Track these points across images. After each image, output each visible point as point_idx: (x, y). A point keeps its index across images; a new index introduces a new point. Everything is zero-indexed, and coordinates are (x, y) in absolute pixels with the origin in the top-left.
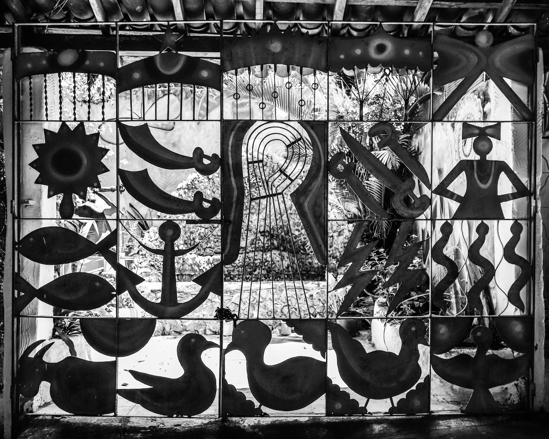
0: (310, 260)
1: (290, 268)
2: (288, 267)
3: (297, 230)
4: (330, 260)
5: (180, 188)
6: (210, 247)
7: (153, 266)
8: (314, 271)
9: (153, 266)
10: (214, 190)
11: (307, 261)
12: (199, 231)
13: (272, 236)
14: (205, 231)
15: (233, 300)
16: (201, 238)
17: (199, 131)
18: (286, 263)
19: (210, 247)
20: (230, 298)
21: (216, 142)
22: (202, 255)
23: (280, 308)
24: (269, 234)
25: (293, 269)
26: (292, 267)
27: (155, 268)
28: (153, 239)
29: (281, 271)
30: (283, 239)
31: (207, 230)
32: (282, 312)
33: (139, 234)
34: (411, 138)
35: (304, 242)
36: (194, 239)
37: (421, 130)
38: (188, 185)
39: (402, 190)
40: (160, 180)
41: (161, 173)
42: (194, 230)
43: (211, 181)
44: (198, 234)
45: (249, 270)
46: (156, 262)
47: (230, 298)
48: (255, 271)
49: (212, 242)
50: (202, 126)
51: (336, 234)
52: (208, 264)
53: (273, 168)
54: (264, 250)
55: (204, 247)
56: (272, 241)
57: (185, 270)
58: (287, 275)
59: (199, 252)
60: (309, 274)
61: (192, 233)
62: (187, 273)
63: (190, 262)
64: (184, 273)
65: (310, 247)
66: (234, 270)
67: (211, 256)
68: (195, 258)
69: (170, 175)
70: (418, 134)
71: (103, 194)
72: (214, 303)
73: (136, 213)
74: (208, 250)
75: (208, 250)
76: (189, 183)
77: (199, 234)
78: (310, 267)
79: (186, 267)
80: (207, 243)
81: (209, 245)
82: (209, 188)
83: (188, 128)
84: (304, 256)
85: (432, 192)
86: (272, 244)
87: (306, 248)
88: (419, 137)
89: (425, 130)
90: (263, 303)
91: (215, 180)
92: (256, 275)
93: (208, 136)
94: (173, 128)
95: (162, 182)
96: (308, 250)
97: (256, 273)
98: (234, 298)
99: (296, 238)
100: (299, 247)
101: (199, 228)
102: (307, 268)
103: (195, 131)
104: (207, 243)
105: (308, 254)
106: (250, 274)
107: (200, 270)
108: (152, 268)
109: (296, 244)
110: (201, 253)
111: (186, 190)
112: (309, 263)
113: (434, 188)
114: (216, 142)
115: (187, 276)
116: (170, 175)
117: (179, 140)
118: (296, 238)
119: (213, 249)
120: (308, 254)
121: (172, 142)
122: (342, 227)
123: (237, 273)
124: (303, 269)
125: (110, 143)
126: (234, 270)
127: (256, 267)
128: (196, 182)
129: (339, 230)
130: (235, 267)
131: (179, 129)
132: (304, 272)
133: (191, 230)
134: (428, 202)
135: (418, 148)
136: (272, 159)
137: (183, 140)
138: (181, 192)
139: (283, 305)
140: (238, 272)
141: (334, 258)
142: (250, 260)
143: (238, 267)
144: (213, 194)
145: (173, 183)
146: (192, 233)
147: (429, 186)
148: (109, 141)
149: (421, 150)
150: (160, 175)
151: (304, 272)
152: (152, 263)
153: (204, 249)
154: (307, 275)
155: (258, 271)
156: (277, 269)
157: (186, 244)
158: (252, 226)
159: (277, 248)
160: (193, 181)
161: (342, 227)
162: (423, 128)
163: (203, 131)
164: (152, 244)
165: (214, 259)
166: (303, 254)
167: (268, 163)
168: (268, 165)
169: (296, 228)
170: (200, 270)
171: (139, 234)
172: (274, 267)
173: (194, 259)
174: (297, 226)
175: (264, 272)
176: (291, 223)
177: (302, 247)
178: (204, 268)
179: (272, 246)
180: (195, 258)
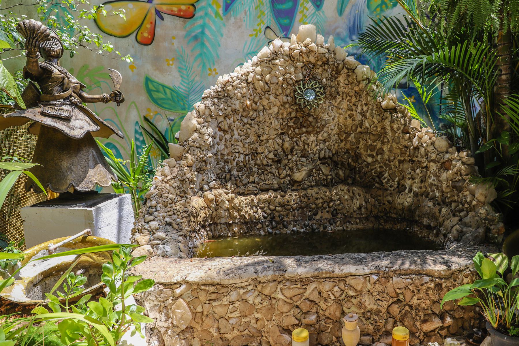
0: (390, 198)
1: (363, 209)
2: (360, 208)
3: (370, 155)
4: (423, 201)
5: (207, 97)
6: (253, 182)
7: (170, 224)
8: (396, 214)
9: (170, 224)
10: (256, 100)
11: (385, 199)
12: (237, 159)
13: (336, 163)
14: (245, 158)
15: (307, 294)
16: (240, 169)
17: (228, 19)
18: (356, 203)
19: (253, 182)
20: (301, 291)
21: (250, 35)
22: (241, 194)
23: (386, 306)
24: (331, 161)
25: (367, 209)
26: (366, 208)
27: (174, 228)
28: (168, 178)
29: (351, 214)
30: (352, 169)
31: (247, 157)
32: (388, 312)
33: (159, 155)
35: (380, 173)
36: (230, 171)
38: (218, 92)
40: (181, 86)
41: (181, 76)
42: (229, 157)
43: (251, 86)
44: (235, 164)
45: (308, 214)
46: (174, 217)
47: (301, 291)
48: (316, 214)
49: (256, 175)
50: (232, 13)
52: (252, 207)
53: (337, 67)
54: (329, 184)
55: (245, 181)
56: (336, 171)
57: (220, 217)
58: (360, 219)
59: (237, 190)
60: (387, 217)
61: (226, 162)
62: (223, 221)
63: (227, 204)
64: (218, 222)
65: (388, 180)
66: (287, 215)
67: (256, 195)
68: (232, 199)
69: (194, 79)
71: (85, 107)
72: (274, 301)
73: (153, 129)
74: (250, 187)
75: (250, 187)
76: (219, 89)
77: (237, 164)
78: (390, 208)
79: (222, 212)
80: (248, 177)
81: (252, 179)
82: (249, 96)
83: (213, 16)
84: (380, 193)
86: (337, 175)
87: (384, 181)
90: (358, 300)
91: (256, 84)
92: (318, 220)
93: (240, 27)
94: (194, 15)
95: (183, 88)
96: (387, 183)
97: (318, 217)
98: (308, 292)
99: (368, 167)
100: (374, 179)
101: (237, 155)
102: (385, 209)
103: (222, 19)
104: (248, 177)
105: (387, 190)
106: (309, 220)
107: (240, 216)
108: (168, 227)
109: (369, 174)
110: (241, 191)
111: (216, 100)
112: (389, 202)
114: (250, 35)
115: (223, 226)
116: (194, 79)
117: (203, 33)
118: (368, 167)
119: (258, 184)
120: (387, 190)
121: (193, 34)
123: (292, 218)
124: (380, 209)
125: (111, 35)
126: (287, 215)
127: (317, 208)
128: (230, 88)
130: (289, 210)
131: (201, 17)
132: (381, 214)
133: (225, 158)
136: (335, 54)
137: (207, 32)
138: (208, 102)
139: (391, 301)
140: (294, 216)
141: (431, 199)
142: (309, 199)
143: (294, 210)
144: (254, 105)
145: (198, 89)
146: (226, 162)
148: (110, 33)
150: (180, 79)
151: (381, 214)
152: (168, 219)
153: (245, 185)
154: (385, 218)
155: (320, 214)
156: (345, 212)
157: (219, 178)
158: (309, 150)
159: (343, 182)
160: (225, 85)
163: (233, 19)
164: (168, 185)
165: (259, 200)
166: (379, 189)
167: (331, 60)
168: (331, 63)
169: (369, 152)
170: (240, 216)
171: (159, 155)
172: (342, 209)
173: (231, 201)
174: (371, 151)
176: (361, 145)
177: (377, 180)
178: (246, 212)
179: (338, 179)
180: (232, 199)
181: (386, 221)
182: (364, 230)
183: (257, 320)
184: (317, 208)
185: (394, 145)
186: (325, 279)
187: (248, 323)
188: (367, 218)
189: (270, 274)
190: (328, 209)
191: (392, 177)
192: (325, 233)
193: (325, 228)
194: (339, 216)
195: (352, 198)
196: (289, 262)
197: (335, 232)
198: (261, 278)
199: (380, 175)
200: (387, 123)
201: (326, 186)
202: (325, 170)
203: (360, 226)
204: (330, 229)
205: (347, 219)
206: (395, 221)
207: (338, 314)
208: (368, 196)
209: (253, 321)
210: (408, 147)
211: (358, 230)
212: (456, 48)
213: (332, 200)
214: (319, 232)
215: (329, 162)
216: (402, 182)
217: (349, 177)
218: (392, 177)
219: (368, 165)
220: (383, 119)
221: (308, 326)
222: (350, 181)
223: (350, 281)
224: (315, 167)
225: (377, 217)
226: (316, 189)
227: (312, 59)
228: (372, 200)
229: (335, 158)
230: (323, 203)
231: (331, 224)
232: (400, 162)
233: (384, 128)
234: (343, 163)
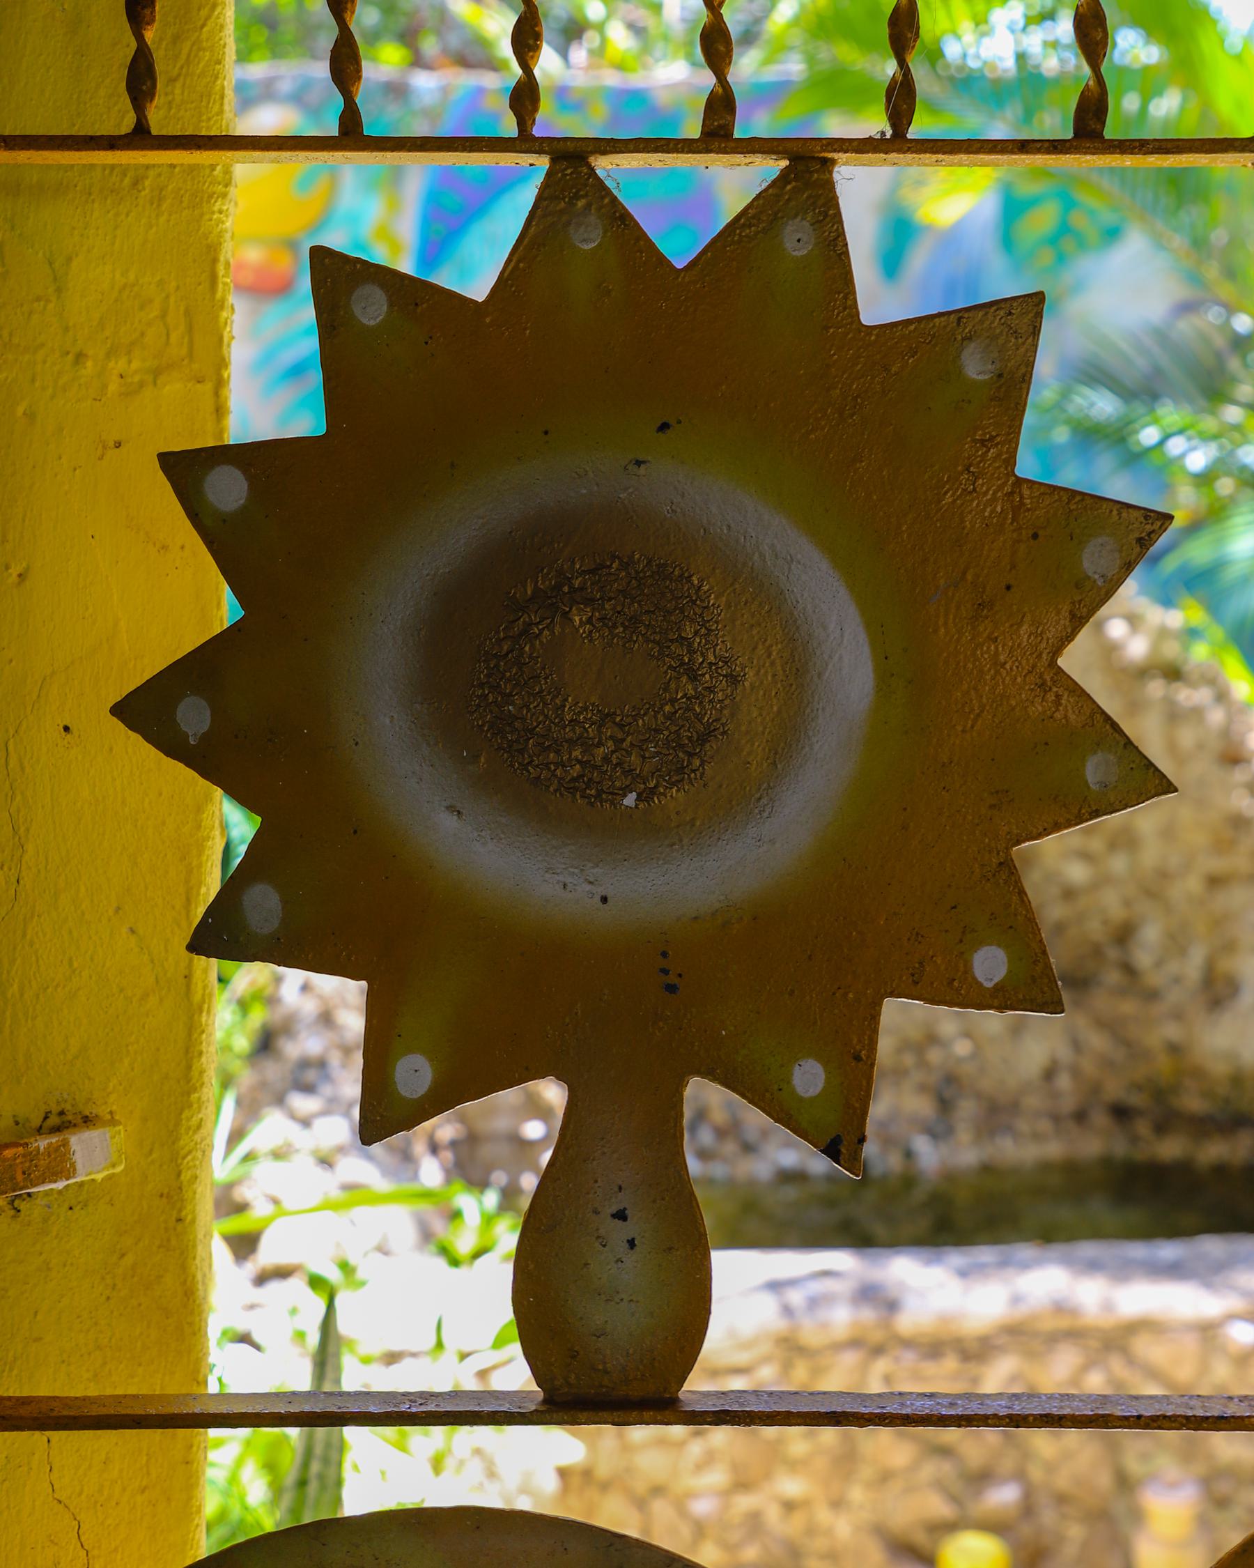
2: (1049, 1074)
26: (1075, 1072)
84: (1128, 1007)
175: (921, 1106)
181: (1162, 1128)
182: (1071, 1169)
183: (789, 1506)
186: (1054, 1339)
187: (754, 1521)
188: (1080, 1116)
189: (842, 1318)
191: (1177, 943)
192: (909, 1181)
193: (909, 1154)
194: (967, 1108)
196: (906, 1271)
197: (950, 1176)
198: (810, 1335)
199: (1124, 934)
203: (1054, 1150)
204: (929, 1155)
205: (998, 1115)
206: (1203, 1126)
207: (1104, 1480)
209: (773, 1515)
216: (1224, 965)
218: (1177, 943)
219: (1069, 894)
221: (995, 1526)
223: (1150, 1350)
225: (1121, 1113)
228: (1097, 1041)
232: (1215, 882)
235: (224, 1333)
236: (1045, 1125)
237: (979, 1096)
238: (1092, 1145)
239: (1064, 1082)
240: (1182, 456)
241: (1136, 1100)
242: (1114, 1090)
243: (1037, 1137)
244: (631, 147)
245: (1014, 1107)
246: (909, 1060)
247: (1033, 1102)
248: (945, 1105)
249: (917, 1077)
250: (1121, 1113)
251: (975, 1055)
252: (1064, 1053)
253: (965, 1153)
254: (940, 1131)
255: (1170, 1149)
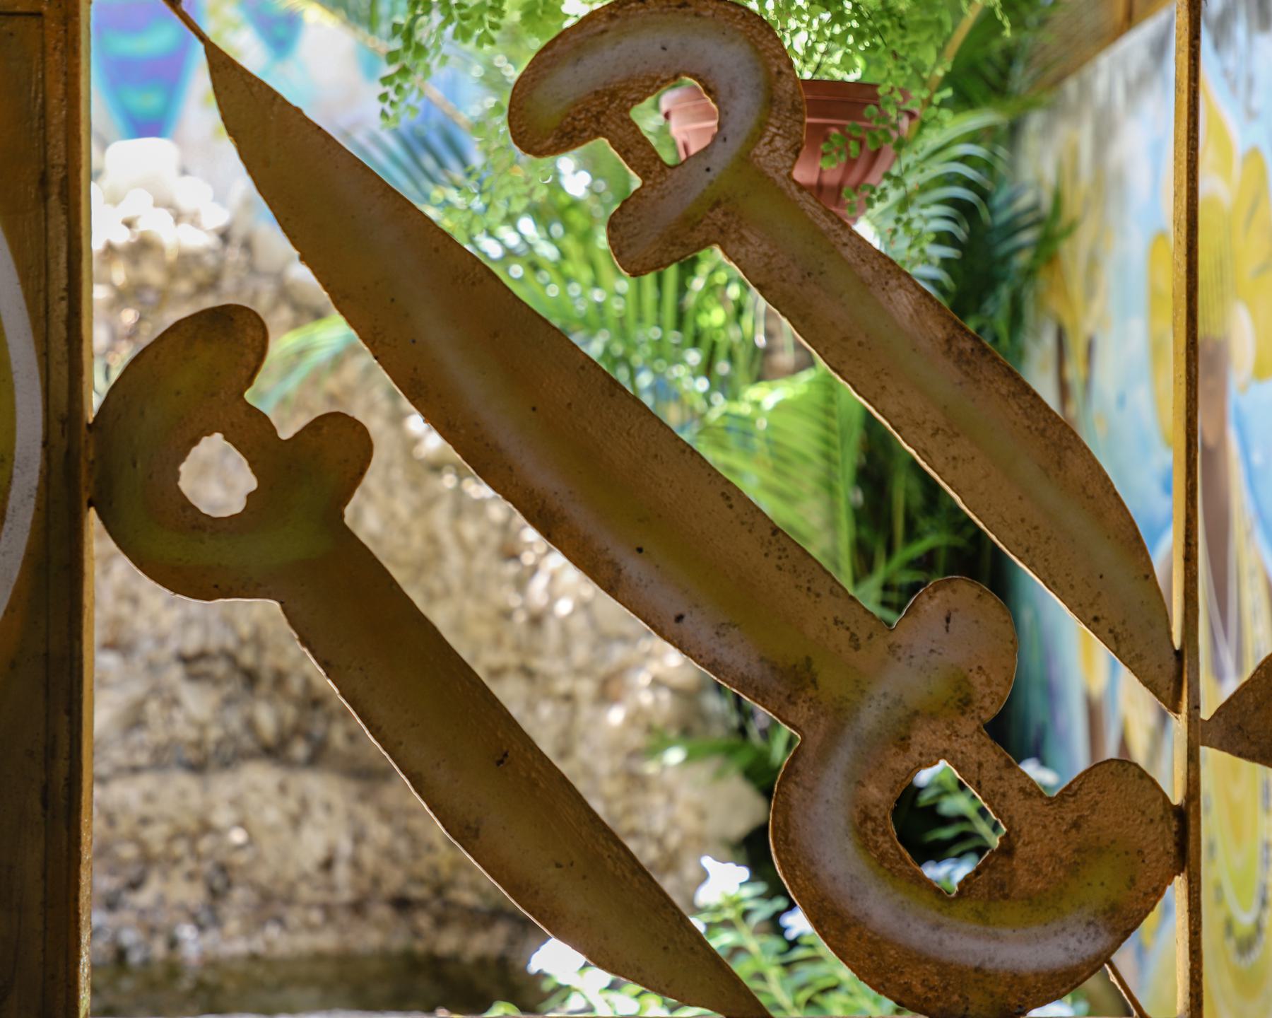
2: (328, 864)
13: (251, 677)
18: (312, 844)
26: (356, 864)
34: (1013, 133)
37: (1071, 86)
39: (869, 717)
48: (135, 885)
51: (586, 688)
58: (327, 909)
70: (1056, 109)
85: (1199, 735)
86: (251, 725)
88: (1064, 131)
89: (1100, 84)
92: (142, 912)
97: (145, 898)
113: (1215, 691)
122: (619, 653)
127: (147, 860)
129: (602, 670)
134: (1161, 838)
135: (1058, 199)
147: (1171, 677)
149: (1072, 207)
159: (274, 752)
161: (619, 653)
162: (1087, 71)
175: (193, 895)
181: (441, 922)
182: (345, 959)
184: (147, 860)
185: (470, 607)
188: (358, 908)
190: (189, 865)
192: (173, 970)
193: (173, 943)
194: (239, 895)
195: (296, 822)
197: (211, 964)
200: (440, 517)
201: (197, 768)
202: (198, 703)
203: (327, 941)
204: (193, 943)
205: (271, 904)
208: (367, 814)
210: (507, 614)
211: (319, 957)
212: (660, 283)
213: (206, 828)
214: (146, 962)
215: (220, 668)
217: (299, 731)
220: (430, 503)
222: (300, 750)
224: (155, 691)
225: (402, 904)
226: (147, 782)
227: (153, 274)
228: (380, 833)
229: (247, 657)
230: (171, 839)
231: (201, 928)
233: (432, 539)
234: (280, 679)
235: (1130, 889)
236: (316, 916)
237: (252, 885)
238: (370, 938)
239: (342, 873)
240: (683, 362)
241: (417, 892)
242: (394, 880)
243: (311, 928)
244: (1192, 766)
245: (290, 900)
246: (180, 848)
247: (305, 892)
248: (216, 895)
249: (189, 865)
250: (402, 904)
251: (251, 841)
252: (345, 846)
253: (233, 941)
254: (207, 919)
255: (448, 942)
